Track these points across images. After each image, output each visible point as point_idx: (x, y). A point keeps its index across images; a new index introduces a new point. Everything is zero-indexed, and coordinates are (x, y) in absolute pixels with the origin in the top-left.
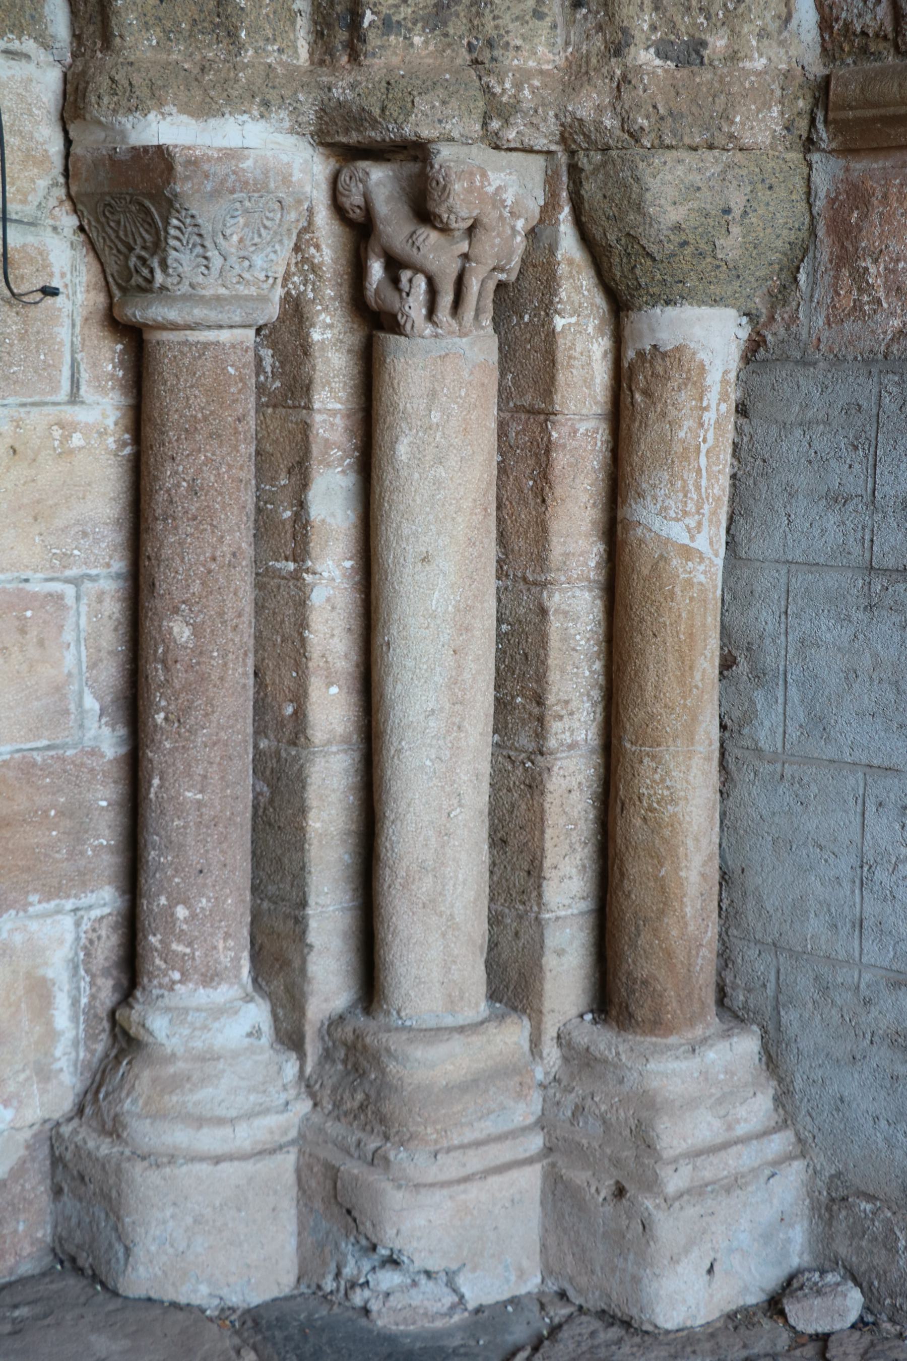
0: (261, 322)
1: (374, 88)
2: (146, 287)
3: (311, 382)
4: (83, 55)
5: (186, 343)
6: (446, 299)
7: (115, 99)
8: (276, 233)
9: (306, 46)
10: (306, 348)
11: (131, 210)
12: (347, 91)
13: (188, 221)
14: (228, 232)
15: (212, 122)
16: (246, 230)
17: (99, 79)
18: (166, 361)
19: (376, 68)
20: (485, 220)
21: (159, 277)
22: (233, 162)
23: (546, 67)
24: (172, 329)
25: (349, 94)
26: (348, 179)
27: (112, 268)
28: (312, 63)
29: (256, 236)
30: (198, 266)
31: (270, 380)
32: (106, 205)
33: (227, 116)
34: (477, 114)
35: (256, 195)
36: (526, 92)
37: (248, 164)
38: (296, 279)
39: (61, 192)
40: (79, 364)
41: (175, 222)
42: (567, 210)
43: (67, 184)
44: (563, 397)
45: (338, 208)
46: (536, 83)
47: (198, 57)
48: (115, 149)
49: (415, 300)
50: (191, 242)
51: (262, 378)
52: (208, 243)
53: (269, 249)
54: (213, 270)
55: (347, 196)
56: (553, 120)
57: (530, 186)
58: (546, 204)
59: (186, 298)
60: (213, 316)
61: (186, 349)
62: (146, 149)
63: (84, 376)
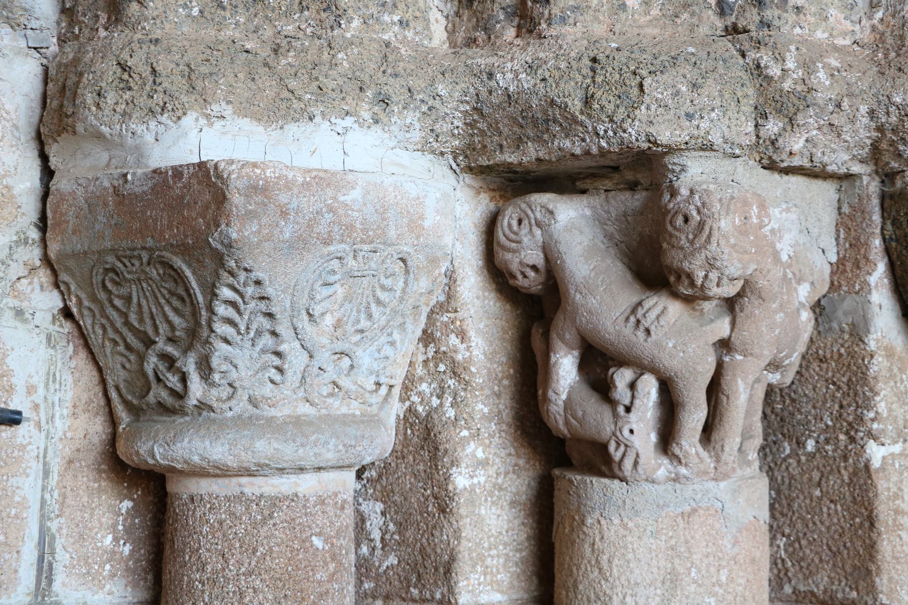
0: (368, 460)
1: (570, 67)
2: (174, 406)
3: (453, 559)
4: (77, 37)
5: (240, 497)
6: (694, 417)
7: (127, 95)
8: (395, 311)
9: (443, 22)
10: (444, 503)
11: (151, 277)
12: (523, 76)
13: (250, 290)
14: (317, 310)
15: (292, 129)
16: (348, 306)
17: (99, 66)
18: (206, 529)
19: (569, 39)
20: (762, 283)
21: (197, 389)
22: (330, 192)
23: (840, 42)
24: (216, 476)
25: (527, 81)
26: (515, 223)
27: (117, 376)
28: (453, 44)
29: (363, 316)
30: (264, 368)
31: (378, 552)
32: (107, 271)
33: (318, 119)
34: (747, 108)
35: (366, 247)
36: (821, 75)
37: (354, 196)
38: (424, 387)
39: (34, 254)
40: (53, 538)
41: (226, 293)
43: (44, 241)
44: (890, 580)
45: (497, 273)
46: (835, 63)
47: (268, 33)
48: (125, 175)
49: (640, 420)
50: (254, 327)
51: (365, 550)
52: (283, 329)
54: (289, 374)
55: (514, 251)
56: (865, 120)
57: (815, 231)
58: (841, 261)
59: (241, 422)
60: (288, 451)
61: (240, 509)
62: (177, 172)
63: (62, 557)
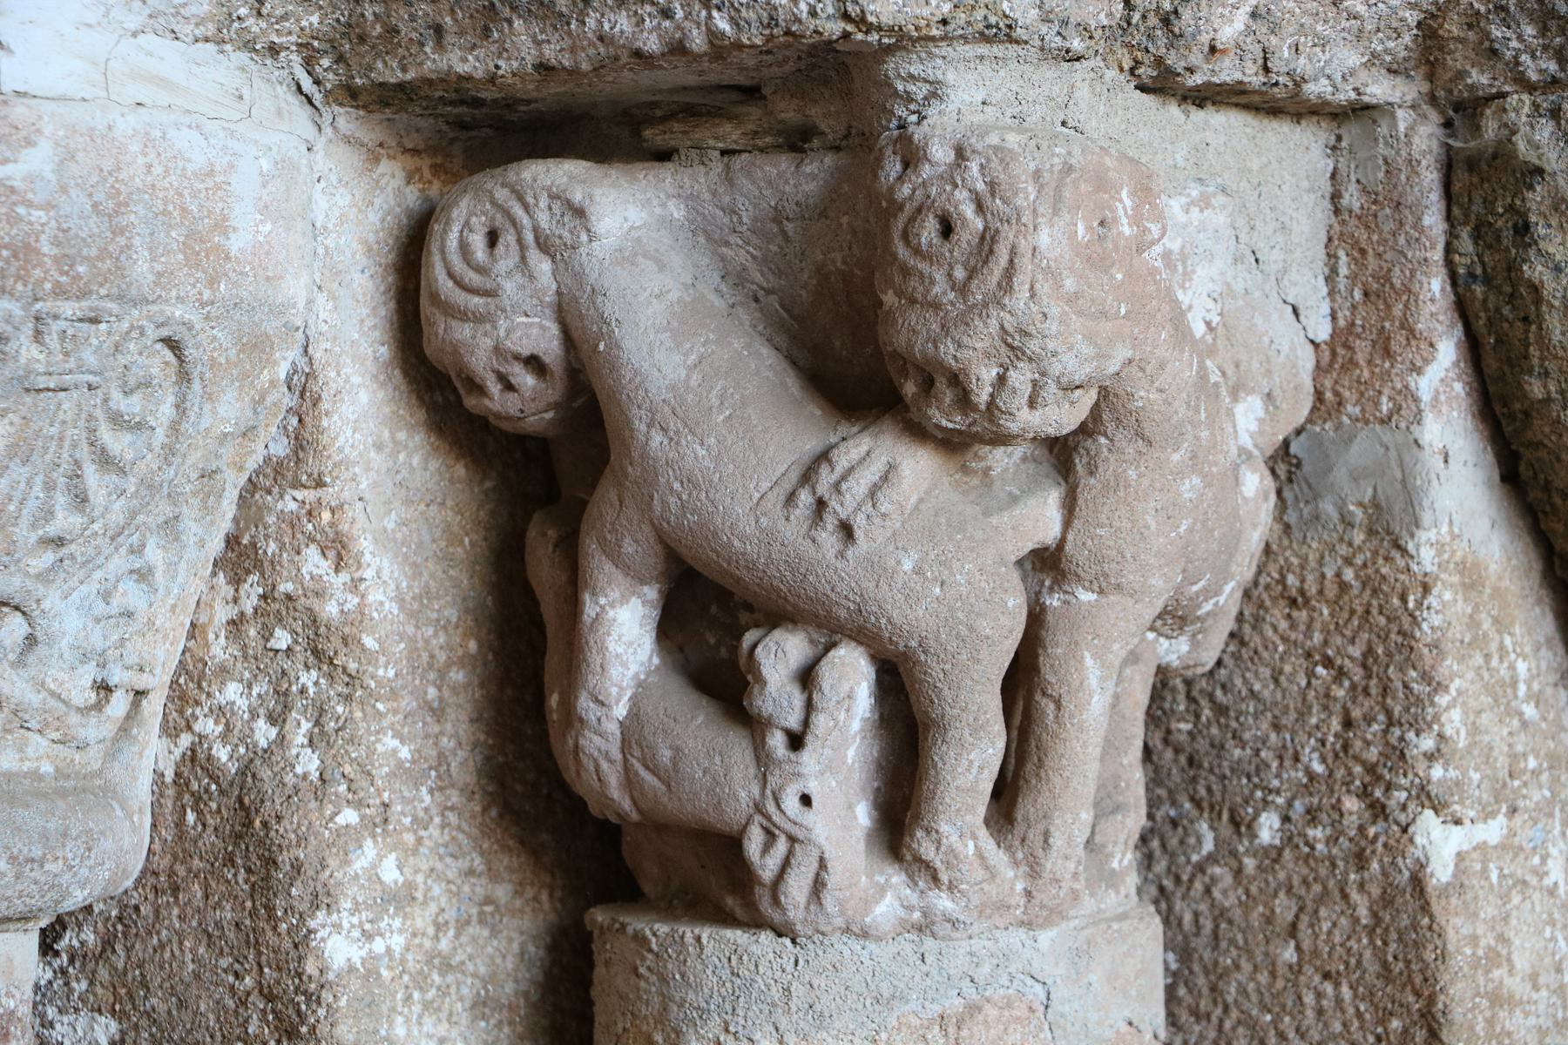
8: (149, 486)
20: (1144, 396)
26: (478, 241)
29: (61, 500)
35: (69, 308)
42: (1447, 352)
45: (432, 381)
49: (829, 768)
53: (119, 563)
55: (479, 319)
57: (1273, 259)
58: (1342, 338)
